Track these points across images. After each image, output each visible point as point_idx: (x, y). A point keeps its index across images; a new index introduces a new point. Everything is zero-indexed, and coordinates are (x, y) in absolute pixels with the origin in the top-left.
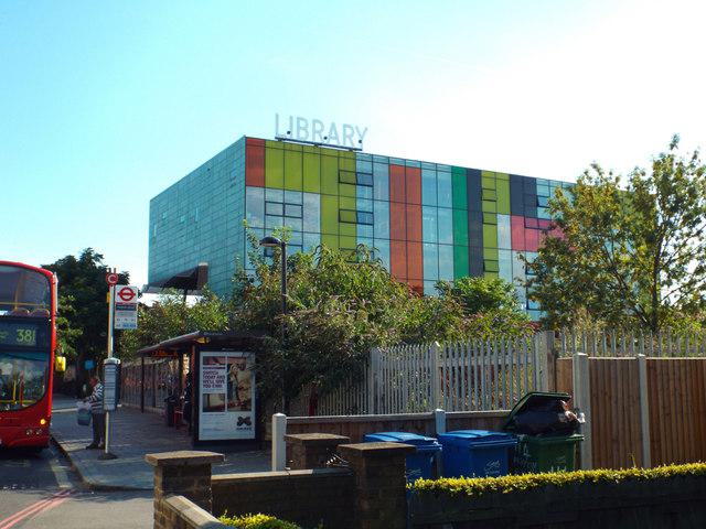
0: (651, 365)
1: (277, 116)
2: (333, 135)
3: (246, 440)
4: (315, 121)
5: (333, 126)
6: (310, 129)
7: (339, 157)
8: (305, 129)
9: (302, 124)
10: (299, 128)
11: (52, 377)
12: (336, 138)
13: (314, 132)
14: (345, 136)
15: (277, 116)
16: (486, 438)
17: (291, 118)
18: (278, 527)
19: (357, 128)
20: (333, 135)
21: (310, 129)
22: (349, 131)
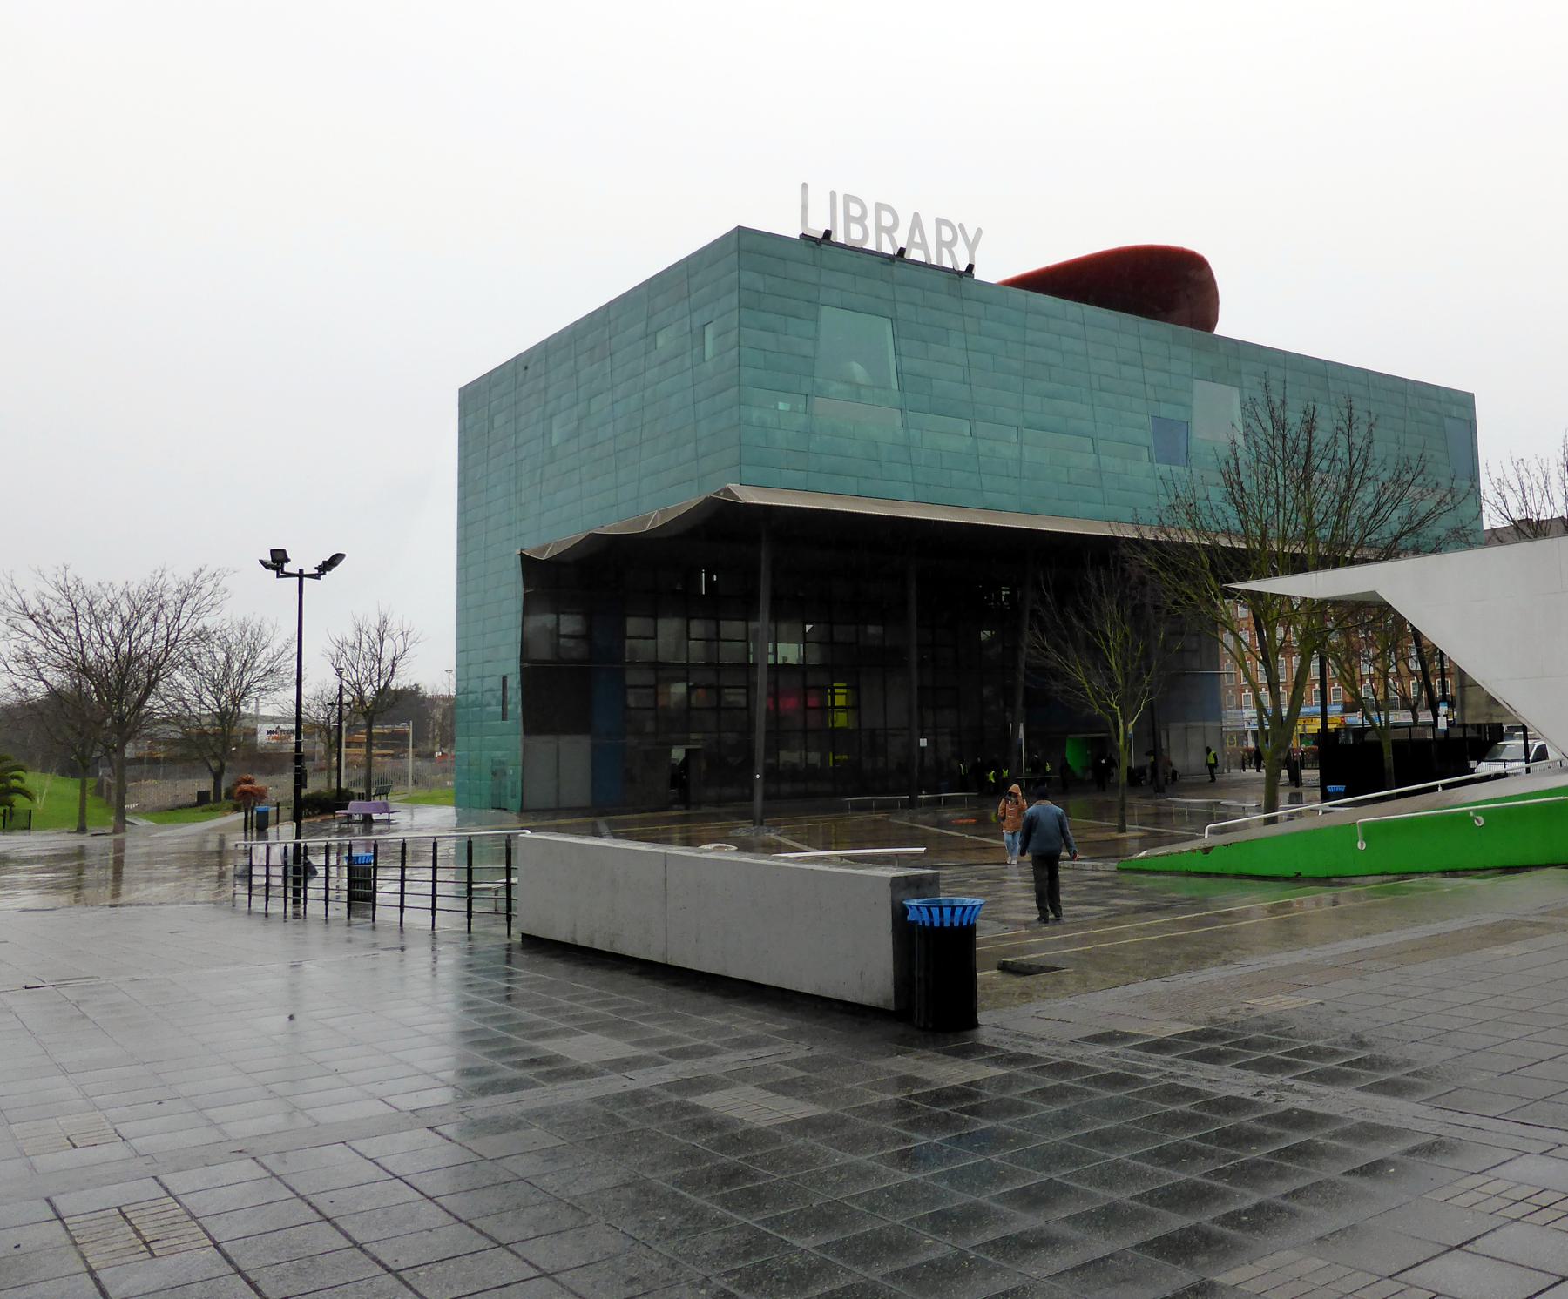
0: (115, 853)
1: (805, 186)
2: (917, 239)
3: (584, 947)
4: (879, 207)
5: (916, 222)
6: (870, 222)
7: (466, 638)
8: (861, 220)
9: (855, 210)
10: (849, 219)
11: (1465, 808)
12: (923, 246)
13: (880, 229)
14: (940, 244)
15: (805, 186)
16: (964, 894)
17: (833, 195)
18: (896, 1296)
19: (961, 226)
20: (917, 239)
21: (870, 222)
22: (947, 235)
